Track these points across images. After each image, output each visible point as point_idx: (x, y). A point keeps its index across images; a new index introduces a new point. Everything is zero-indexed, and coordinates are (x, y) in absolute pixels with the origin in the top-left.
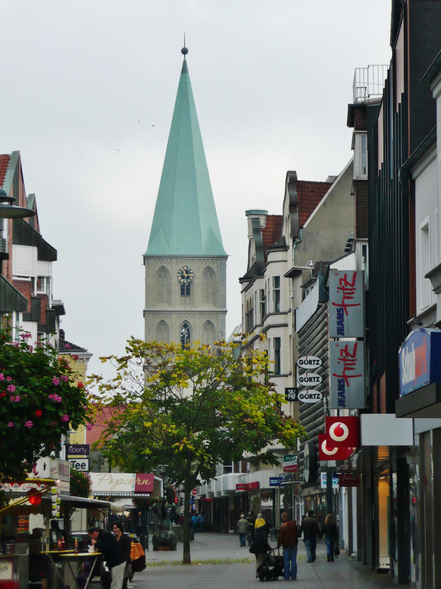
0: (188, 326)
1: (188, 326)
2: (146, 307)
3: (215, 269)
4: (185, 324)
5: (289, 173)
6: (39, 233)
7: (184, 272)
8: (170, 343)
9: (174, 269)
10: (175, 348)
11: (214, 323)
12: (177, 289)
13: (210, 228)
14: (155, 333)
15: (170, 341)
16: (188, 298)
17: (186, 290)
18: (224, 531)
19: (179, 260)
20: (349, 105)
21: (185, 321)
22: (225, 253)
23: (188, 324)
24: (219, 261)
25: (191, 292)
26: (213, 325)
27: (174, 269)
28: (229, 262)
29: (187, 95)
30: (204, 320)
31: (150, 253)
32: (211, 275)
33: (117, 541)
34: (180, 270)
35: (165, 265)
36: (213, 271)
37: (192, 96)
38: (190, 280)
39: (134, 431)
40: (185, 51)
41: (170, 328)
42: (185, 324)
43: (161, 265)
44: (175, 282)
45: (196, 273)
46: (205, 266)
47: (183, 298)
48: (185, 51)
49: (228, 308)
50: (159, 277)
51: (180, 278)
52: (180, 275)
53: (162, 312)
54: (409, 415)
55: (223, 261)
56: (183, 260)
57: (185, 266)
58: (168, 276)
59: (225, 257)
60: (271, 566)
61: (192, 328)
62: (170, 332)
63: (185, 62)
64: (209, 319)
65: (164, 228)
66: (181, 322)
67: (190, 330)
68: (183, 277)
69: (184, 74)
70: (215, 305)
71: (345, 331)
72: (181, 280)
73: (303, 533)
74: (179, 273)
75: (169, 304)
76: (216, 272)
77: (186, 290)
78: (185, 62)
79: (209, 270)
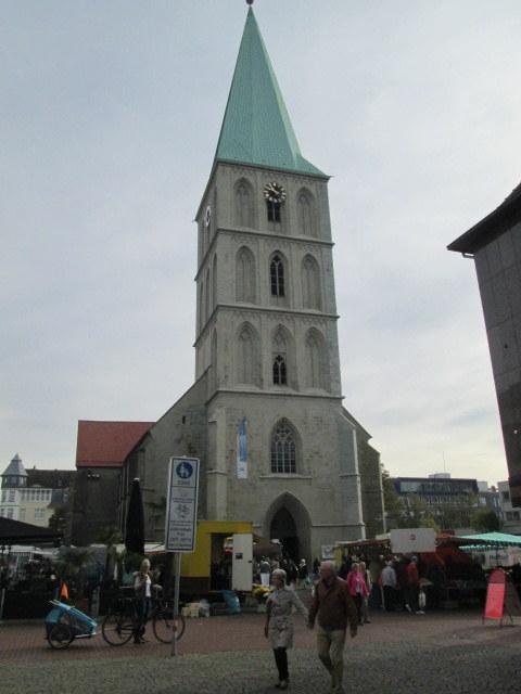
6: (315, 172)
10: (193, 615)
12: (262, 209)
16: (278, 225)
20: (80, 422)
21: (277, 251)
23: (279, 256)
24: (318, 183)
27: (261, 185)
28: (330, 184)
29: (267, 68)
30: (303, 253)
36: (311, 195)
37: (283, 103)
46: (300, 186)
47: (271, 224)
54: (296, 167)
61: (287, 262)
63: (250, 13)
66: (271, 252)
67: (284, 265)
68: (272, 194)
77: (278, 287)
79: (309, 259)
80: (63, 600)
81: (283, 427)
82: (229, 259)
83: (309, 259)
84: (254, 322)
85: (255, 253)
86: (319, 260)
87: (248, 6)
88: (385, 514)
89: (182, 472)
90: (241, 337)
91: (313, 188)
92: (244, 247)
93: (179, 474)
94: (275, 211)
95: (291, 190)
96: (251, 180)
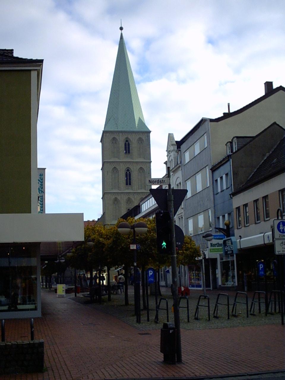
0: (129, 170)
1: (129, 170)
3: (144, 139)
4: (128, 169)
5: (169, 134)
11: (145, 169)
13: (140, 118)
14: (110, 174)
17: (128, 182)
21: (128, 167)
22: (148, 129)
23: (129, 169)
26: (144, 170)
28: (151, 134)
31: (107, 130)
32: (141, 143)
33: (165, 242)
35: (115, 136)
40: (121, 29)
42: (128, 169)
43: (113, 137)
44: (122, 145)
48: (121, 29)
49: (152, 160)
53: (115, 163)
58: (117, 143)
59: (150, 132)
60: (137, 264)
63: (122, 34)
65: (113, 117)
66: (124, 138)
67: (131, 173)
69: (121, 40)
70: (145, 159)
75: (119, 159)
76: (145, 140)
77: (128, 182)
78: (122, 34)
79: (140, 140)
80: (20, 304)
81: (120, 218)
82: (109, 173)
83: (140, 140)
84: (119, 197)
85: (119, 170)
86: (145, 169)
87: (120, 31)
88: (230, 265)
89: (281, 228)
90: (114, 203)
91: (144, 137)
92: (115, 167)
93: (279, 230)
94: (127, 148)
95: (134, 140)
96: (117, 138)
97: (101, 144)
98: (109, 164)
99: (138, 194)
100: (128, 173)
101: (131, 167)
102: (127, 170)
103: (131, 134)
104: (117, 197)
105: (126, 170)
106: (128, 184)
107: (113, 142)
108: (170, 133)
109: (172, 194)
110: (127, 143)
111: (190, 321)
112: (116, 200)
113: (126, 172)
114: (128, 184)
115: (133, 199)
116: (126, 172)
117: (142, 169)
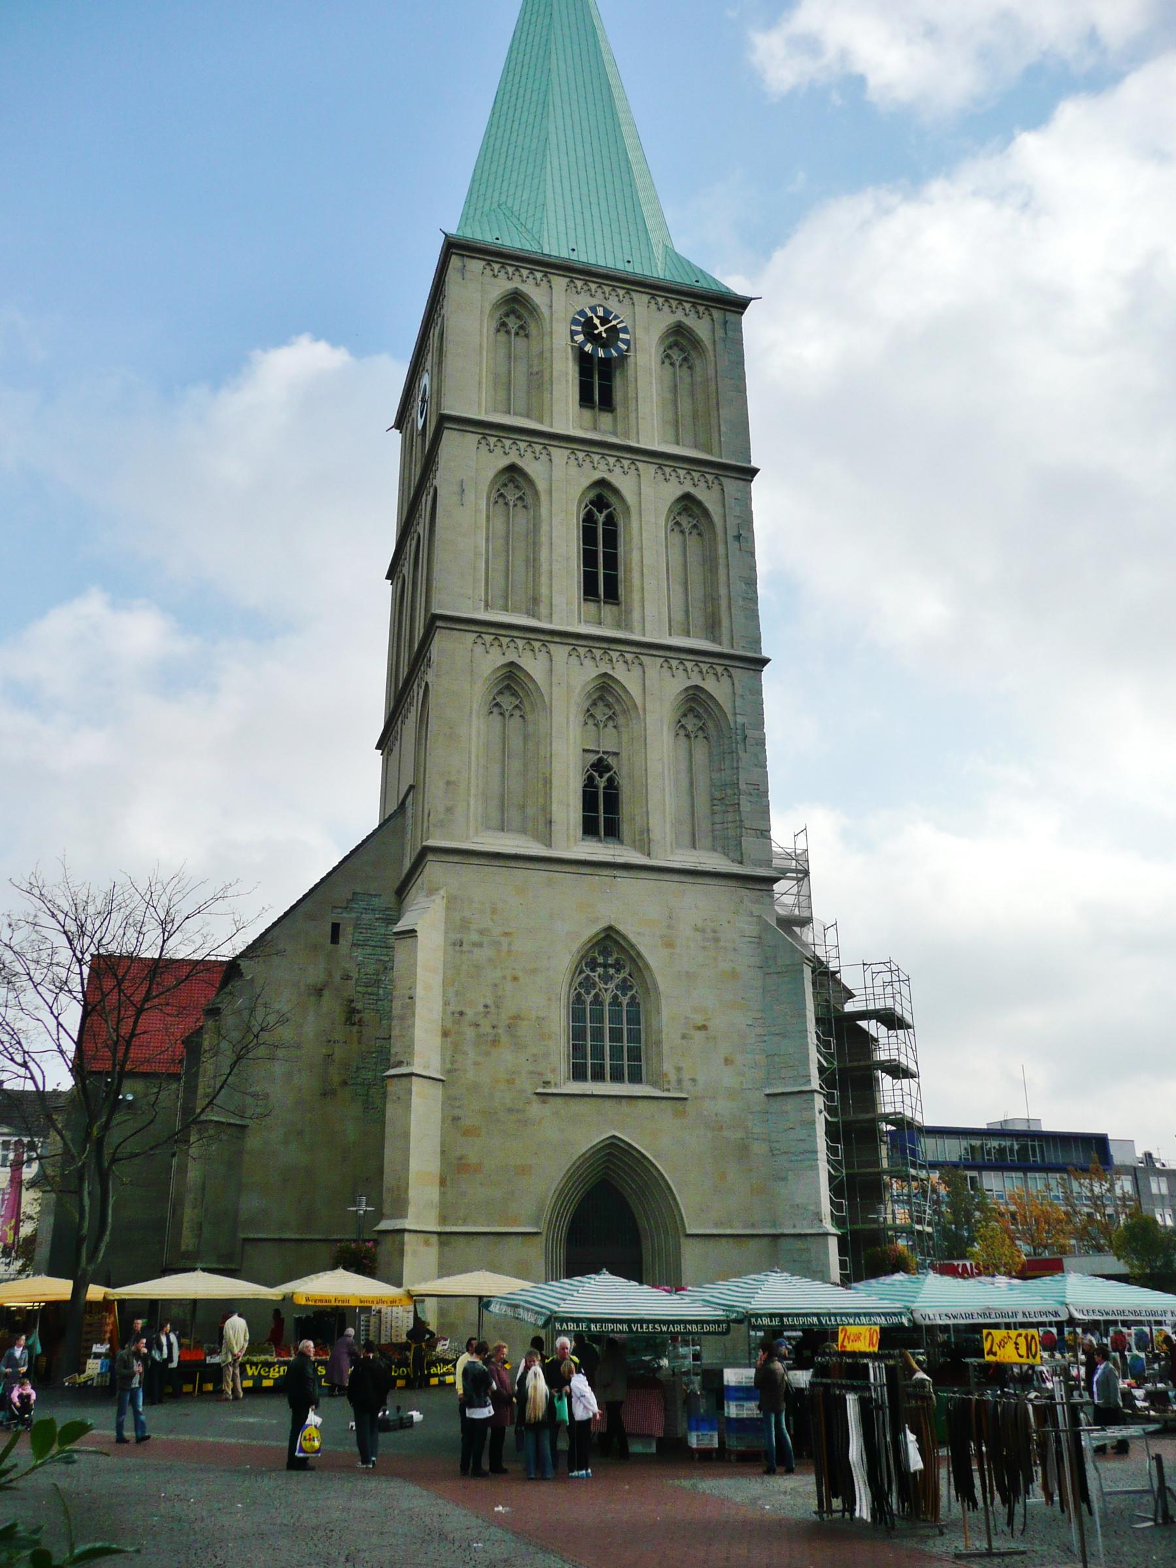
2: (465, 218)
7: (596, 321)
8: (658, 252)
9: (560, 306)
15: (654, 237)
18: (783, 1469)
19: (579, 284)
23: (613, 500)
24: (716, 314)
25: (618, 396)
27: (560, 306)
30: (672, 490)
32: (685, 359)
34: (582, 313)
38: (618, 349)
39: (1011, 1381)
41: (544, 497)
45: (639, 333)
50: (498, 331)
51: (580, 338)
52: (579, 329)
55: (731, 317)
56: (593, 286)
57: (600, 306)
62: (544, 510)
64: (692, 490)
71: (625, 828)
72: (583, 344)
73: (968, 1360)
74: (575, 322)
85: (541, 485)
95: (645, 328)
97: (387, 587)
98: (471, 439)
99: (667, 659)
100: (601, 518)
101: (623, 482)
102: (592, 503)
103: (628, 291)
104: (522, 662)
105: (587, 500)
106: (608, 1076)
107: (504, 324)
108: (1136, 1143)
109: (1115, 1351)
110: (602, 783)
111: (1154, 1463)
112: (512, 681)
113: (579, 999)
114: (608, 1076)
115: (634, 689)
116: (573, 993)
117: (697, 511)
